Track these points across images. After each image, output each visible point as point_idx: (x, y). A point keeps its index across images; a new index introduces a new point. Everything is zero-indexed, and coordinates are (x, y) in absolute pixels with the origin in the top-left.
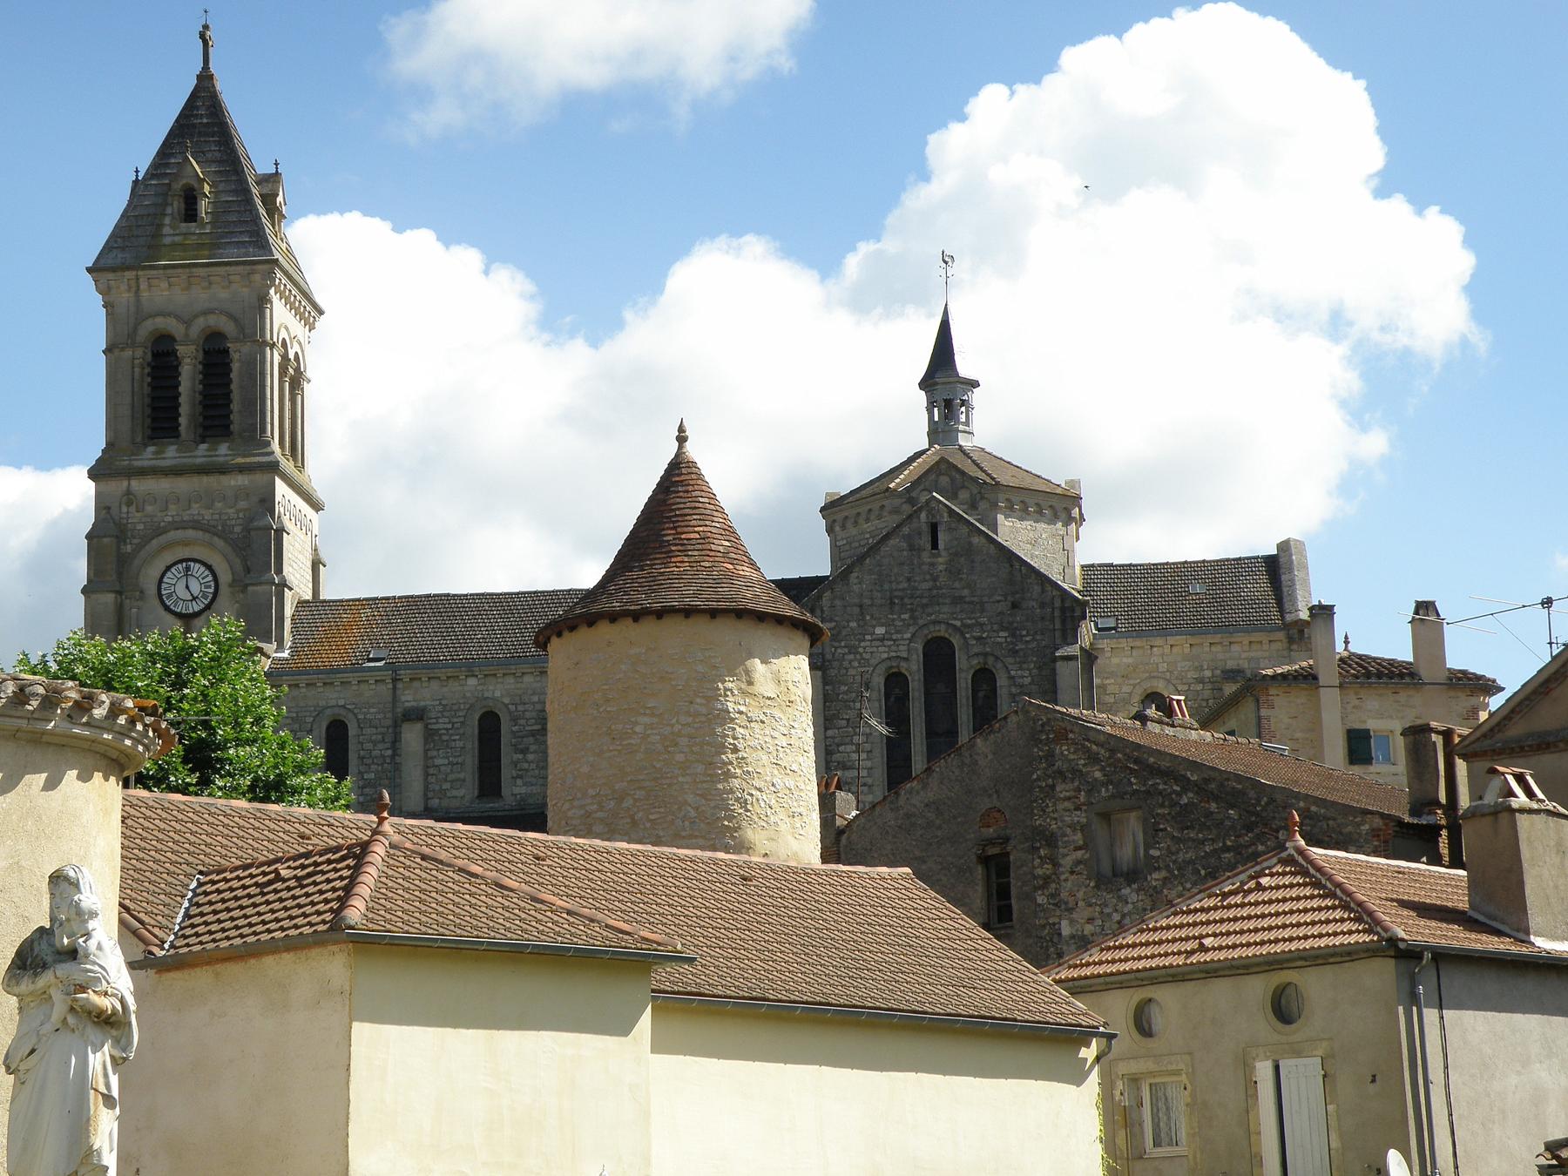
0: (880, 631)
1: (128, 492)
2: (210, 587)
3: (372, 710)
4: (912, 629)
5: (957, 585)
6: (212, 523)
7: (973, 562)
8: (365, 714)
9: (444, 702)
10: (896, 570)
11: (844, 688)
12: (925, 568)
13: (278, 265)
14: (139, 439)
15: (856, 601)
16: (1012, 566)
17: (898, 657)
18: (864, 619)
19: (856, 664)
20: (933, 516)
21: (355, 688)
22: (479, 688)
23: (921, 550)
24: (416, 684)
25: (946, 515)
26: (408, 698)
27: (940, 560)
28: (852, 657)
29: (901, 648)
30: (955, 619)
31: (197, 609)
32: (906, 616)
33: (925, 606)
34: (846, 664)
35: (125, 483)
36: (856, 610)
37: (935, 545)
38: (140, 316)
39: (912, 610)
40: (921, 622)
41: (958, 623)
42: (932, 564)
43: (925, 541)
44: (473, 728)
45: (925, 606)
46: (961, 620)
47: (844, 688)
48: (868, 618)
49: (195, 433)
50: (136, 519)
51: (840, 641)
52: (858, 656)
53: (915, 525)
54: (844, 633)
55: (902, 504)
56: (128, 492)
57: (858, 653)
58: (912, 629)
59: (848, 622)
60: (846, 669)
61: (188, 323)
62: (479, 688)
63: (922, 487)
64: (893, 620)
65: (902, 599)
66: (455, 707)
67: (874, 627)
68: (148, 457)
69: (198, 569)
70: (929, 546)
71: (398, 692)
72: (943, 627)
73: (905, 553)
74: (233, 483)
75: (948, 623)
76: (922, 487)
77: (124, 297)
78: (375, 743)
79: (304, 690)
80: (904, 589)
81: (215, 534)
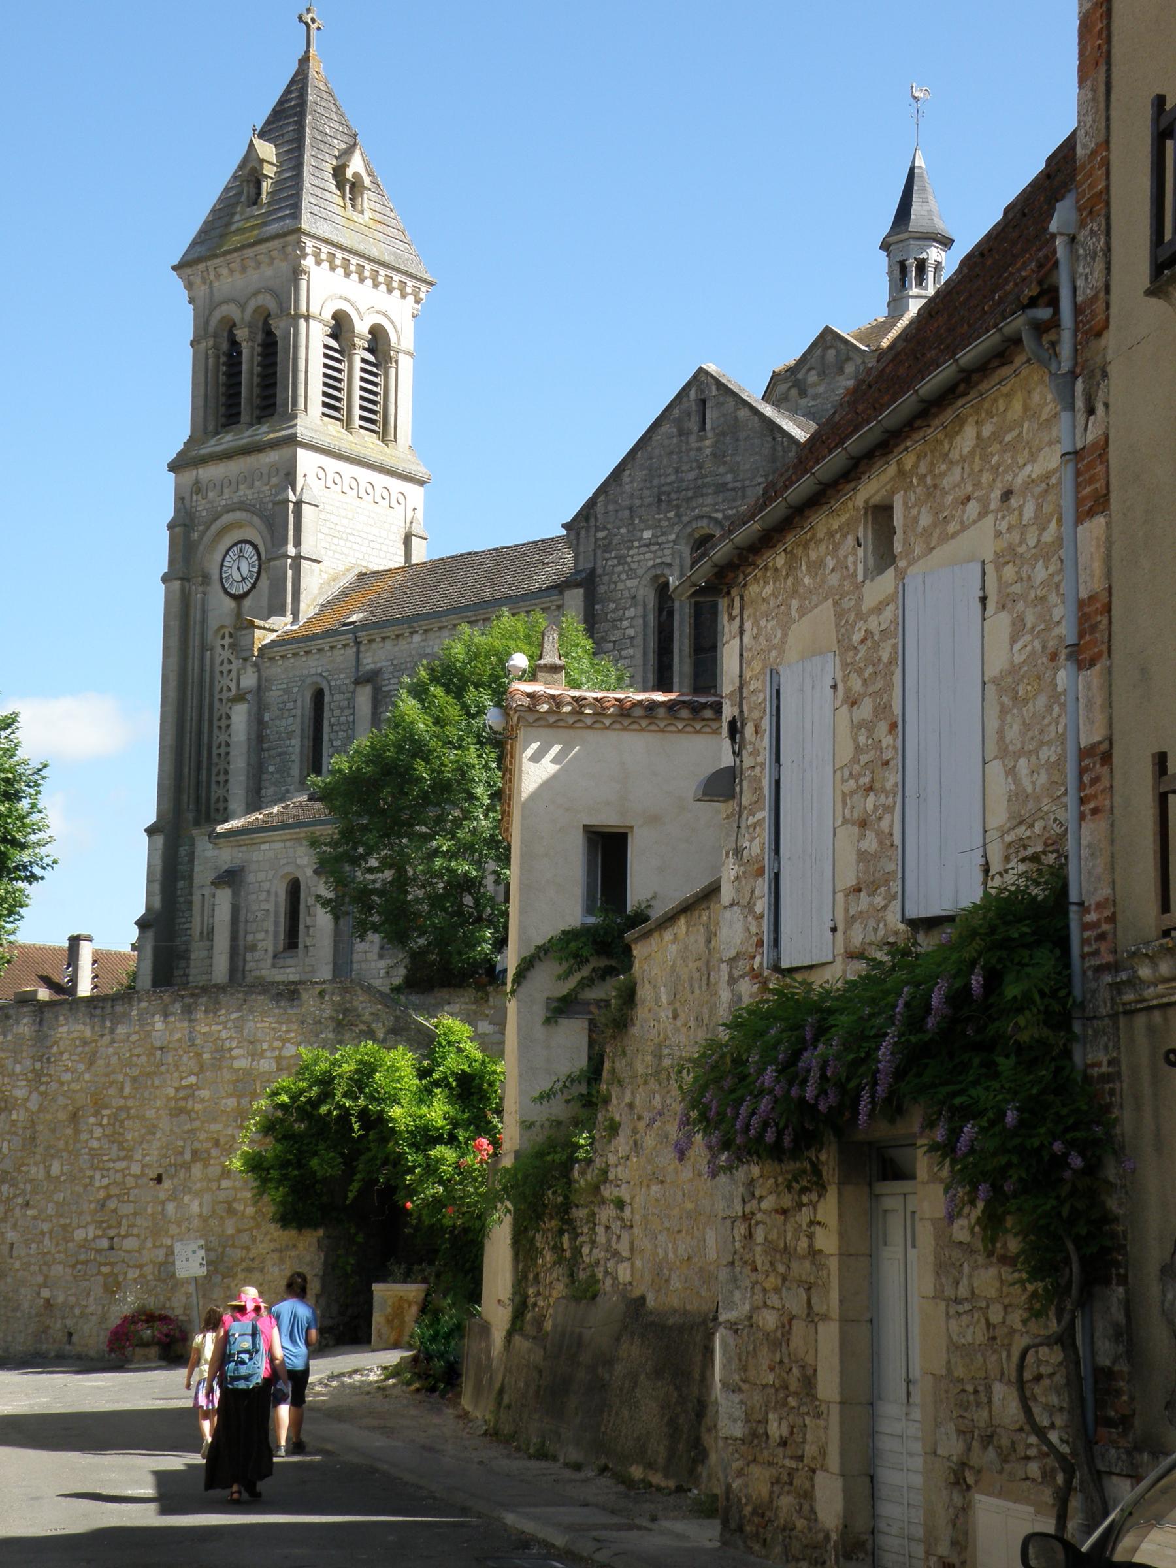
0: (647, 534)
1: (197, 482)
2: (253, 567)
3: (342, 676)
4: (677, 529)
5: (722, 470)
6: (253, 502)
7: (737, 440)
8: (336, 680)
9: (395, 662)
10: (665, 462)
11: (612, 606)
12: (692, 454)
13: (305, 234)
14: (211, 428)
15: (627, 503)
16: (774, 439)
17: (663, 563)
18: (633, 523)
19: (624, 576)
20: (702, 391)
21: (329, 654)
22: (422, 644)
23: (688, 434)
24: (374, 646)
25: (714, 388)
26: (369, 662)
27: (707, 443)
28: (620, 568)
29: (667, 552)
30: (717, 511)
31: (246, 589)
32: (671, 514)
33: (689, 500)
34: (615, 578)
35: (195, 472)
36: (627, 513)
37: (703, 428)
38: (213, 306)
39: (678, 507)
40: (685, 519)
41: (719, 516)
42: (699, 449)
43: (693, 424)
44: (308, 695)
45: (689, 500)
46: (723, 511)
47: (612, 606)
48: (637, 521)
49: (252, 414)
50: (201, 507)
51: (610, 552)
52: (626, 567)
53: (685, 405)
54: (615, 542)
55: (789, 388)
56: (197, 482)
57: (626, 563)
58: (677, 529)
59: (619, 528)
60: (615, 583)
61: (243, 307)
62: (422, 644)
63: (807, 367)
64: (660, 520)
65: (669, 494)
66: (403, 667)
67: (642, 530)
68: (228, 440)
69: (249, 550)
70: (696, 428)
71: (361, 655)
72: (704, 522)
73: (675, 440)
74: (267, 460)
75: (710, 517)
76: (807, 367)
77: (202, 290)
78: (342, 709)
79: (292, 660)
80: (670, 484)
81: (253, 513)
